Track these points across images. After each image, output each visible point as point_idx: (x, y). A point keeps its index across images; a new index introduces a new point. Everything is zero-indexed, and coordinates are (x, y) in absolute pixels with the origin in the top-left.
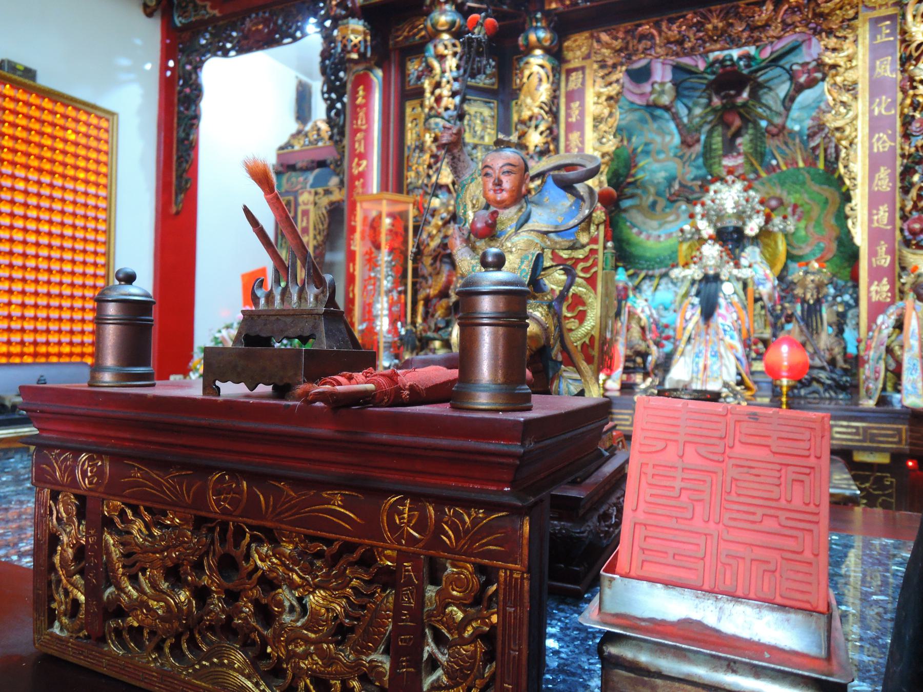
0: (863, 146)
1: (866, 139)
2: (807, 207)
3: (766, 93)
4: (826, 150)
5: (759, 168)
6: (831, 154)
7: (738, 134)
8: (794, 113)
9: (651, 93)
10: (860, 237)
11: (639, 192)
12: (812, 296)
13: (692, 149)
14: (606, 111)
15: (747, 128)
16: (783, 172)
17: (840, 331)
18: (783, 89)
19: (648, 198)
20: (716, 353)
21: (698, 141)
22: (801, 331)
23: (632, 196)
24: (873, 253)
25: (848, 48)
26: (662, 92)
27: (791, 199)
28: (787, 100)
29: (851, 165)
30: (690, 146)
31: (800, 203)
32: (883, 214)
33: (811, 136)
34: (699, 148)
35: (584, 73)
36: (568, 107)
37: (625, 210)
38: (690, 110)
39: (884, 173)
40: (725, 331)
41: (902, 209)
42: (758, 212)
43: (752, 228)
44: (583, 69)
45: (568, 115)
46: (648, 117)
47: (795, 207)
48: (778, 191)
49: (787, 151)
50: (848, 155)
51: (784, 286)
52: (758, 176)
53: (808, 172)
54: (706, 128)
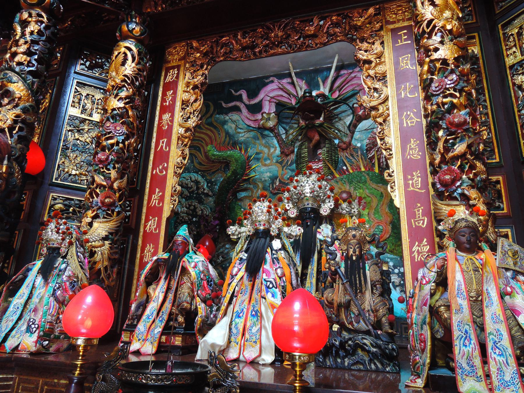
0: (394, 122)
1: (397, 116)
2: (369, 199)
3: (337, 122)
4: (379, 160)
6: (383, 162)
7: (317, 146)
8: (357, 135)
9: (261, 120)
10: (399, 201)
11: (252, 186)
12: (354, 252)
13: (289, 157)
14: (193, 99)
15: (324, 143)
17: (386, 293)
18: (348, 120)
19: (257, 191)
20: (256, 312)
21: (293, 152)
22: (345, 289)
23: (245, 190)
24: (411, 215)
25: (377, 47)
26: (269, 119)
27: (358, 193)
28: (351, 127)
29: (387, 139)
30: (287, 155)
31: (363, 196)
32: (417, 181)
33: (369, 150)
34: (293, 157)
35: (178, 70)
36: (164, 94)
37: (241, 200)
38: (287, 131)
39: (413, 143)
40: (268, 287)
41: (432, 164)
42: (329, 197)
43: (325, 209)
44: (178, 67)
45: (163, 100)
46: (259, 135)
47: (360, 199)
48: (347, 187)
49: (353, 160)
52: (334, 177)
53: (368, 174)
54: (298, 144)
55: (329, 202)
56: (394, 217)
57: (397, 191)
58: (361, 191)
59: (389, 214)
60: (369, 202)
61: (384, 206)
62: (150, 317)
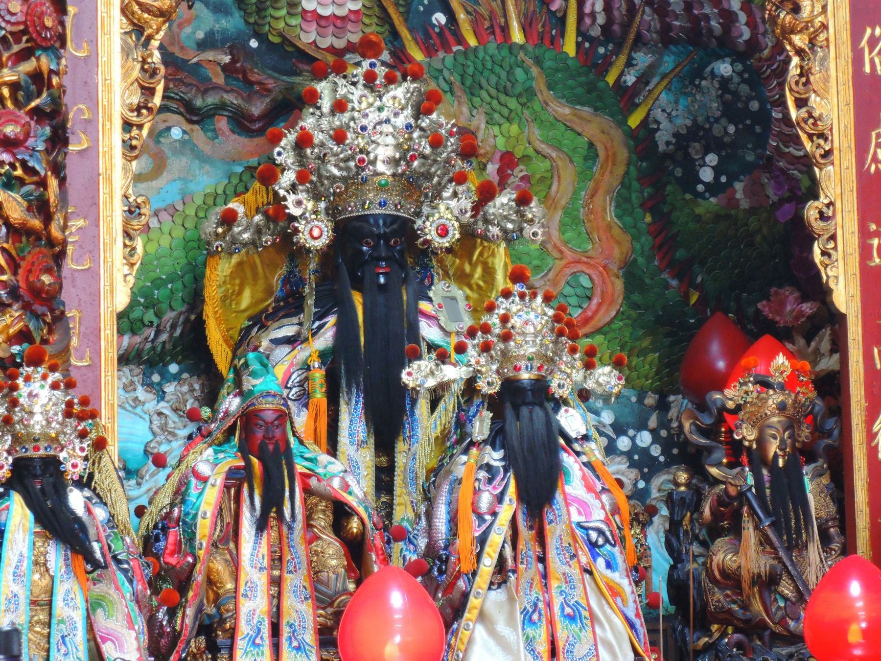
2: (541, 167)
5: (404, 32)
6: (593, 15)
16: (468, 51)
40: (593, 545)
47: (508, 161)
50: (805, 73)
51: (707, 420)
53: (538, 61)
55: (455, 194)
56: (638, 246)
57: (841, 263)
58: (514, 129)
59: (617, 232)
60: (543, 179)
61: (599, 198)
62: (258, 641)
